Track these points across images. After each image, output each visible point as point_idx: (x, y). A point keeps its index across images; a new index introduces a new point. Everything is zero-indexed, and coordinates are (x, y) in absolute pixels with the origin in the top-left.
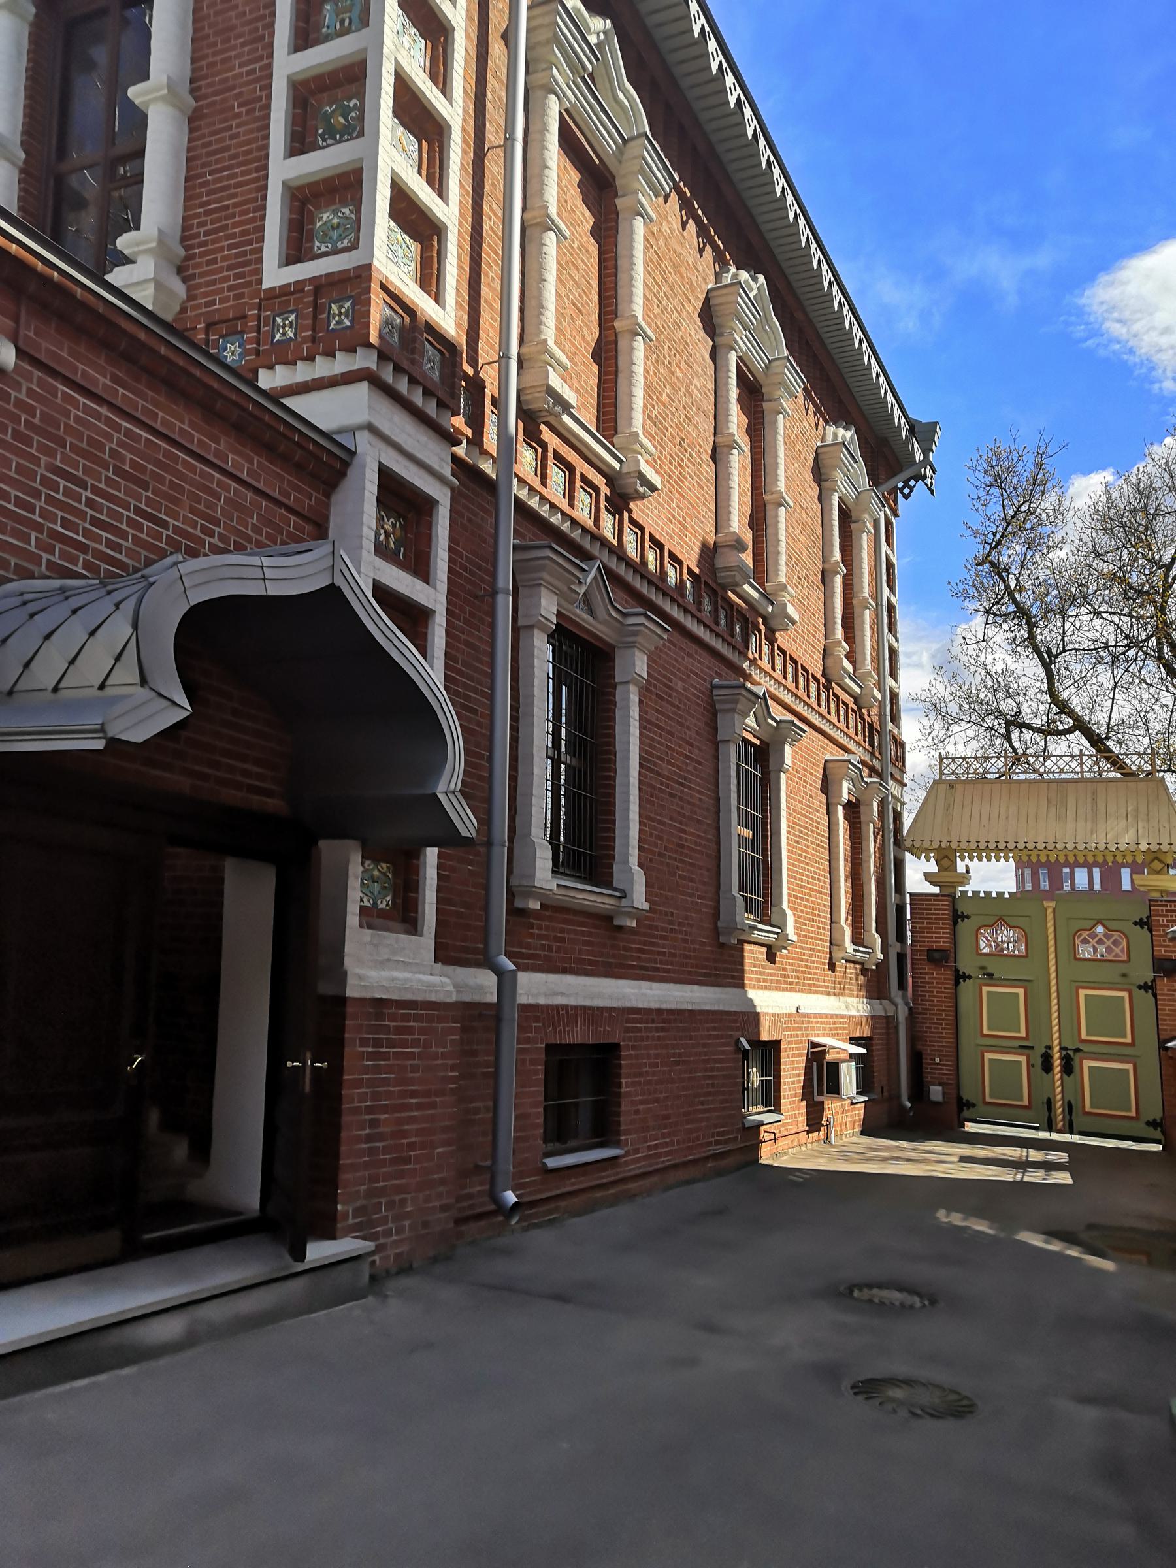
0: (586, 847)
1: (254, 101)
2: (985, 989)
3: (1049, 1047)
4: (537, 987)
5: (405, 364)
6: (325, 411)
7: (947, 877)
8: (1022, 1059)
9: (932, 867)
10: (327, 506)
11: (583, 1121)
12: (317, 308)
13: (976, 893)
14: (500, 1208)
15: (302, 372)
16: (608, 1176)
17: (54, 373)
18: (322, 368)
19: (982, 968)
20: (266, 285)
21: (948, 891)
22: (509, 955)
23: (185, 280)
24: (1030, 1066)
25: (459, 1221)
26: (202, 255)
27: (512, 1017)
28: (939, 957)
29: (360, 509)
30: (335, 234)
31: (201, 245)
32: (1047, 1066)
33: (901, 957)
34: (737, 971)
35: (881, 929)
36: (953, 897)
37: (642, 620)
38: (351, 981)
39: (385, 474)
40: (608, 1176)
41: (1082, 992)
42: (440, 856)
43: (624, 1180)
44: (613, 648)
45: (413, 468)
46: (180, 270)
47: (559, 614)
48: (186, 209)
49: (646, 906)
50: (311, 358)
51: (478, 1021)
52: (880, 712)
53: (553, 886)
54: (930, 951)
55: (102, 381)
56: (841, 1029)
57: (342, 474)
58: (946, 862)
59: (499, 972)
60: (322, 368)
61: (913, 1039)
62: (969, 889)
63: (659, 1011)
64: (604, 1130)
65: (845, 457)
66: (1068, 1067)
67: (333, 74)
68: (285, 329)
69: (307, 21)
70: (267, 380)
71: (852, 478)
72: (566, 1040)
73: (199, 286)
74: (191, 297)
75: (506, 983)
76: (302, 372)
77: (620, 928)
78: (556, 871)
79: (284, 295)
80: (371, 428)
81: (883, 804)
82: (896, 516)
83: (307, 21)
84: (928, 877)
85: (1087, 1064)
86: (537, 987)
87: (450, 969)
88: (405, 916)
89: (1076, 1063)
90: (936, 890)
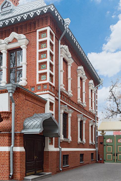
0: (66, 136)
1: (34, 64)
2: (107, 147)
3: (114, 153)
4: (64, 149)
5: (51, 91)
6: (43, 97)
7: (103, 133)
8: (111, 155)
9: (101, 132)
10: (45, 106)
11: (65, 162)
12: (43, 86)
13: (106, 135)
14: (60, 170)
15: (41, 93)
16: (68, 168)
17: (27, 100)
18: (43, 92)
19: (107, 144)
20: (37, 84)
21: (103, 135)
22: (60, 146)
23: (27, 82)
24: (112, 155)
25: (57, 172)
26: (29, 79)
27: (61, 152)
28: (101, 143)
29: (48, 106)
30: (44, 78)
31: (29, 78)
32: (114, 155)
33: (97, 143)
34: (55, 142)
35: (95, 140)
36: (103, 136)
37: (71, 111)
38: (49, 150)
39: (50, 102)
40: (68, 168)
41: (119, 146)
42: (55, 138)
43: (69, 168)
44: (68, 113)
45: (52, 101)
46: (26, 81)
47: (64, 112)
48: (27, 74)
49: (71, 140)
50: (42, 91)
51: (58, 153)
52: (88, 87)
53: (63, 139)
54: (101, 142)
55: (30, 100)
56: (23, 165)
57: (46, 103)
58: (103, 132)
59: (60, 148)
60: (43, 92)
61: (98, 153)
62: (105, 135)
63: (72, 151)
64: (67, 164)
65: (92, 85)
66: (116, 156)
67: (43, 62)
68: (39, 88)
69: (40, 56)
70: (37, 93)
71: (92, 87)
72: (65, 154)
73: (29, 82)
74: (28, 84)
75: (60, 149)
76: (41, 93)
77: (69, 143)
78: (64, 138)
79: (39, 85)
80: (49, 98)
81: (95, 125)
82: (98, 89)
83: (40, 56)
84: (101, 134)
85: (119, 155)
86: (64, 149)
87: (56, 148)
88: (51, 143)
89: (117, 155)
90: (101, 135)
